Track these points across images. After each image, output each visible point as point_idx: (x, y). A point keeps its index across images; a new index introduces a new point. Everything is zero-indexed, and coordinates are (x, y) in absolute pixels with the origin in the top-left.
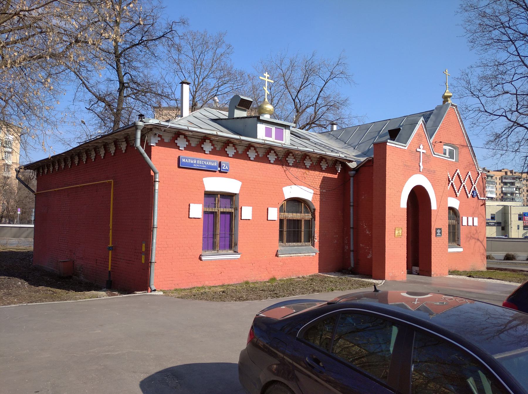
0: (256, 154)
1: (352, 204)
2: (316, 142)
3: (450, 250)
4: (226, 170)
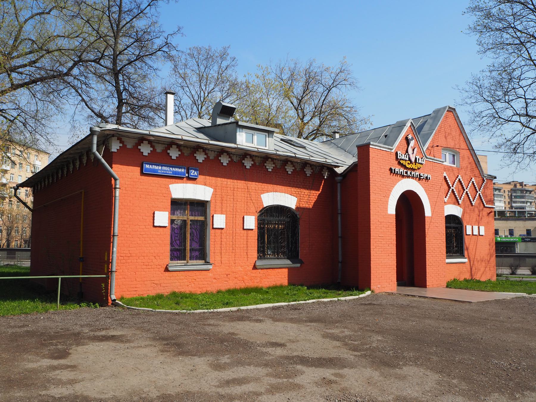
0: (294, 168)
1: (339, 211)
2: (317, 151)
3: (448, 261)
4: (195, 176)
